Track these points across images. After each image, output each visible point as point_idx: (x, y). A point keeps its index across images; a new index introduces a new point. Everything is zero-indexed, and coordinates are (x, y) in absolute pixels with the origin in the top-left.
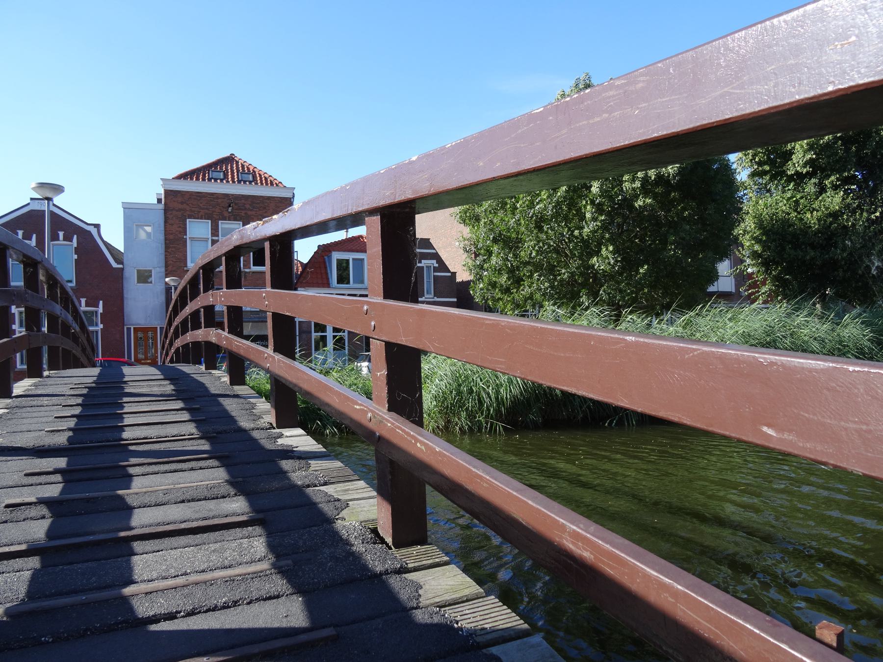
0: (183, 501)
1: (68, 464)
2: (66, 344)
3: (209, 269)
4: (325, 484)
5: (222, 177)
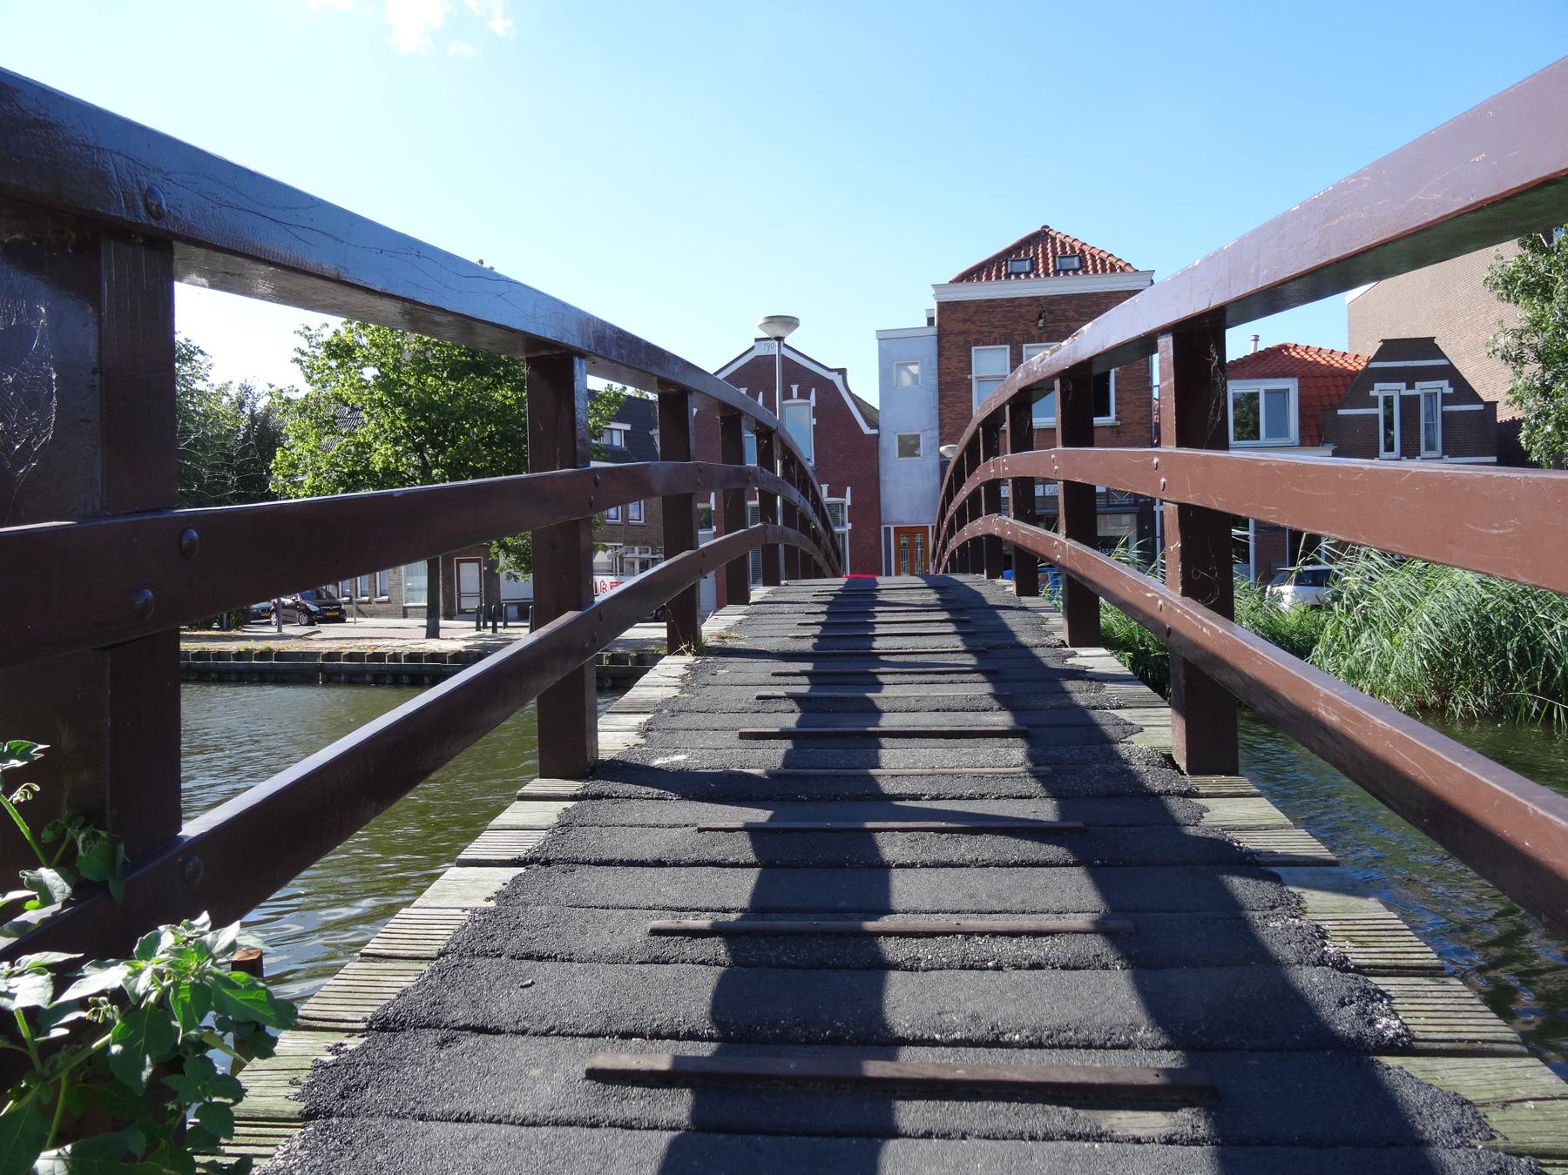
0: (938, 710)
1: (814, 667)
2: (807, 546)
3: (991, 424)
4: (1119, 707)
5: (1028, 268)
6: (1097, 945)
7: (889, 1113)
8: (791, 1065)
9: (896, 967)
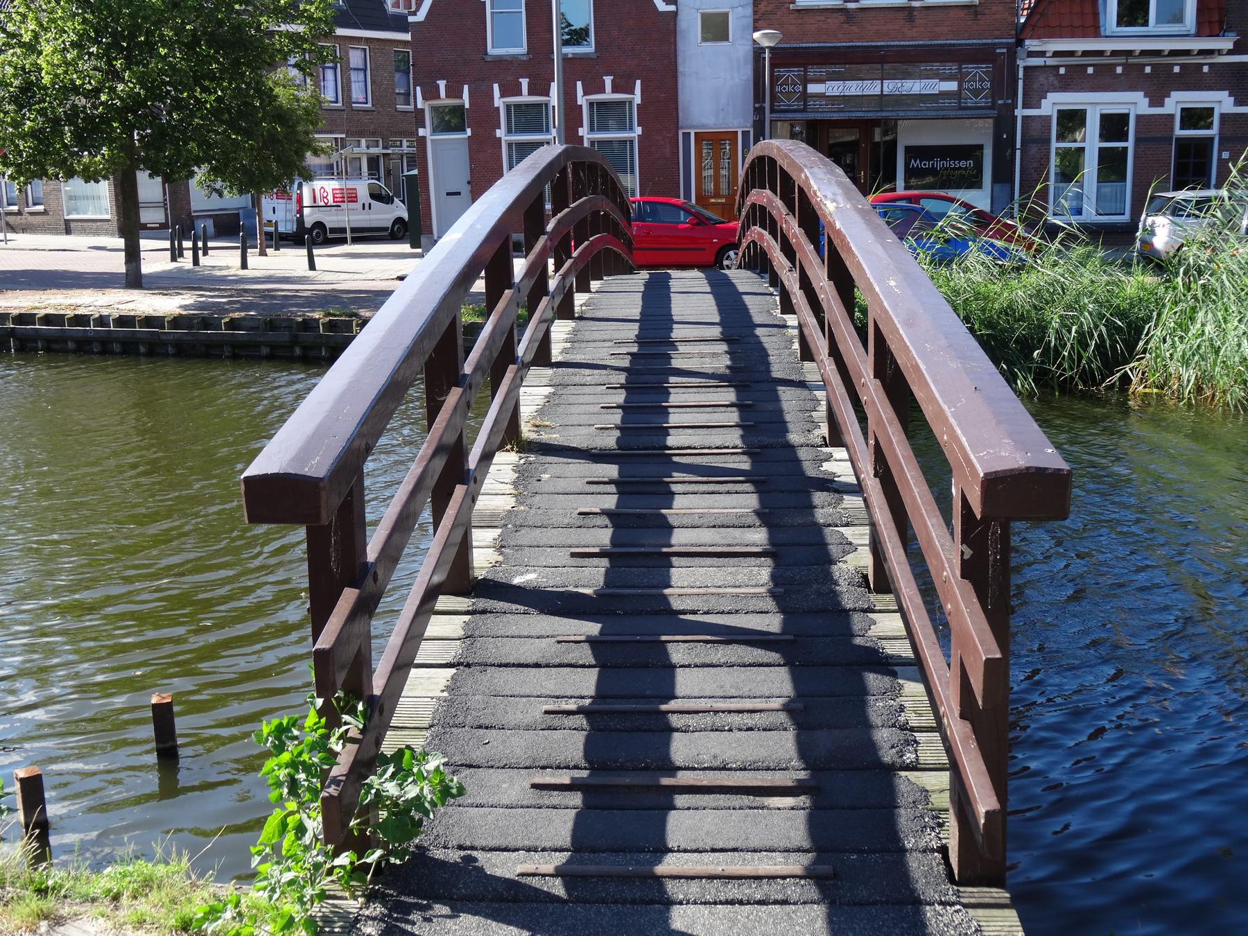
0: (714, 527)
4: (847, 525)
6: (783, 717)
7: (672, 800)
8: (627, 780)
9: (677, 730)
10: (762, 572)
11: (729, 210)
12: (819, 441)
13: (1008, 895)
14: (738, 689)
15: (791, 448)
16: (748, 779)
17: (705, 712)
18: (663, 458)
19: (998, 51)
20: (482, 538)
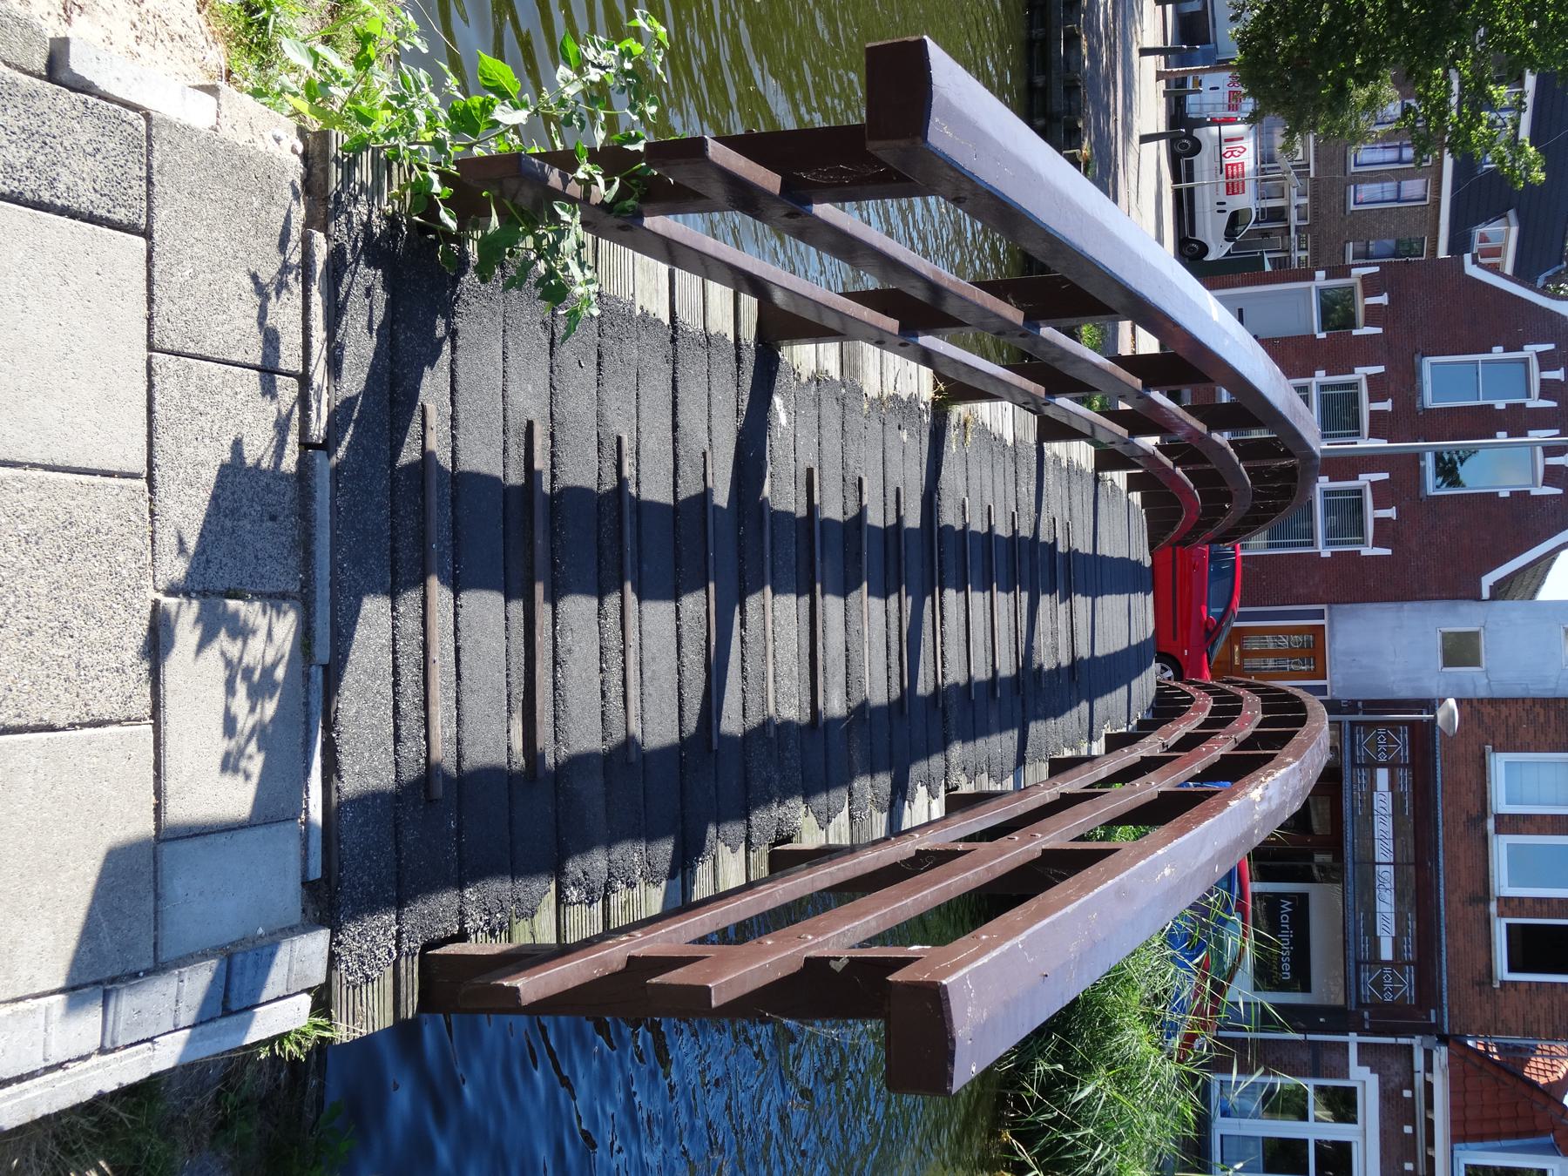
0: (847, 650)
4: (851, 817)
6: (618, 736)
7: (516, 597)
8: (540, 541)
9: (601, 604)
10: (792, 710)
11: (1224, 669)
12: (953, 782)
13: (410, 1015)
14: (652, 679)
15: (944, 747)
16: (544, 693)
17: (623, 638)
18: (928, 585)
19: (1433, 1012)
20: (829, 355)
